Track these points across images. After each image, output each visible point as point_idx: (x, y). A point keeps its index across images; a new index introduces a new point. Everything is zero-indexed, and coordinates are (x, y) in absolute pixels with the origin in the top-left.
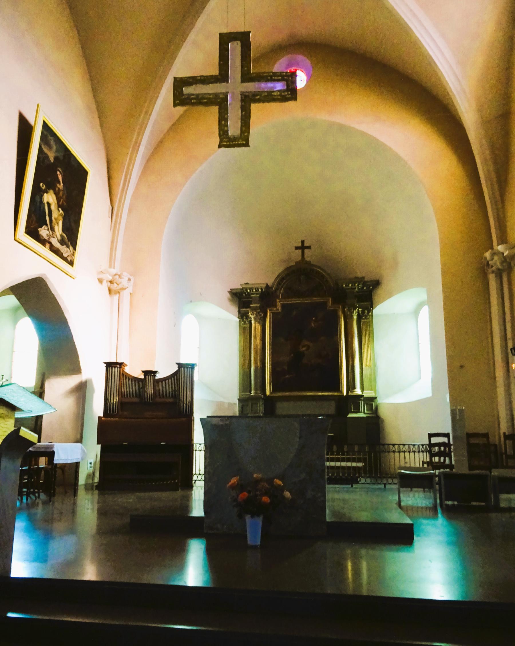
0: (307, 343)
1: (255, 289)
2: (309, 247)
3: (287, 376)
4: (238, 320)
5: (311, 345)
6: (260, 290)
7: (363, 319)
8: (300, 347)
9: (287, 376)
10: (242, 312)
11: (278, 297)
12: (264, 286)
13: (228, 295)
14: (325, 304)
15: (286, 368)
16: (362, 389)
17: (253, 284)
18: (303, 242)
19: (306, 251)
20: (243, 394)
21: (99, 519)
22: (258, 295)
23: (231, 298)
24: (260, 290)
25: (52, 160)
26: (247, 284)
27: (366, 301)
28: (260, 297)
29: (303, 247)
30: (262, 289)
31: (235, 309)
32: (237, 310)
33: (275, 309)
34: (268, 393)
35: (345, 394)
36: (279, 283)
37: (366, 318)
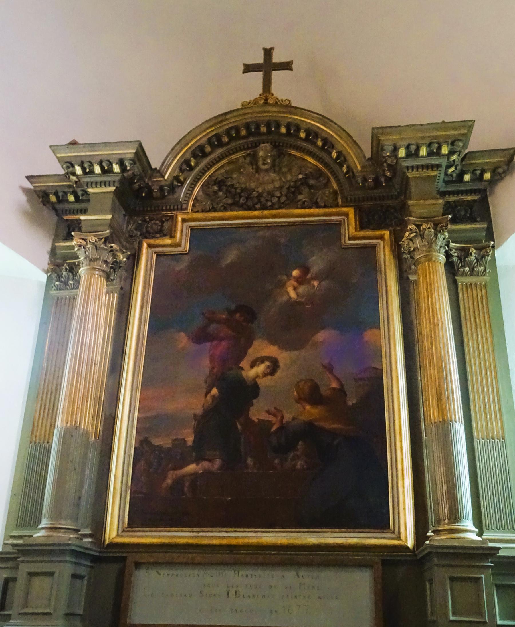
0: (272, 350)
1: (101, 164)
2: (287, 66)
3: (192, 468)
4: (44, 278)
5: (284, 357)
6: (116, 168)
7: (464, 274)
8: (245, 364)
9: (192, 468)
10: (59, 252)
11: (181, 209)
12: (130, 152)
13: (23, 198)
14: (335, 228)
15: (190, 440)
16: (478, 522)
17: (92, 146)
18: (268, 53)
19: (276, 75)
20: (15, 533)
21: (303, 285)
22: (113, 189)
23: (28, 207)
24: (116, 168)
25: (180, 346)
26: (74, 143)
27: (473, 220)
28: (119, 194)
29: (268, 66)
30: (121, 163)
31: (41, 244)
32: (48, 247)
33: (168, 241)
34: (112, 531)
35: (410, 543)
36: (186, 166)
37: (472, 272)
